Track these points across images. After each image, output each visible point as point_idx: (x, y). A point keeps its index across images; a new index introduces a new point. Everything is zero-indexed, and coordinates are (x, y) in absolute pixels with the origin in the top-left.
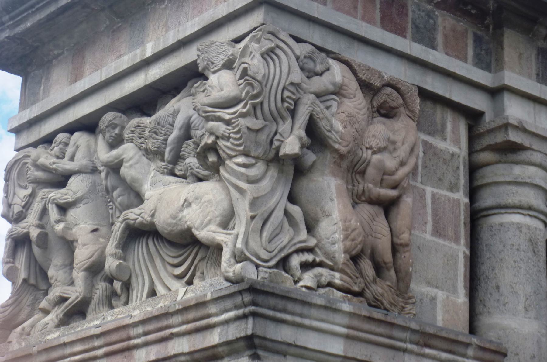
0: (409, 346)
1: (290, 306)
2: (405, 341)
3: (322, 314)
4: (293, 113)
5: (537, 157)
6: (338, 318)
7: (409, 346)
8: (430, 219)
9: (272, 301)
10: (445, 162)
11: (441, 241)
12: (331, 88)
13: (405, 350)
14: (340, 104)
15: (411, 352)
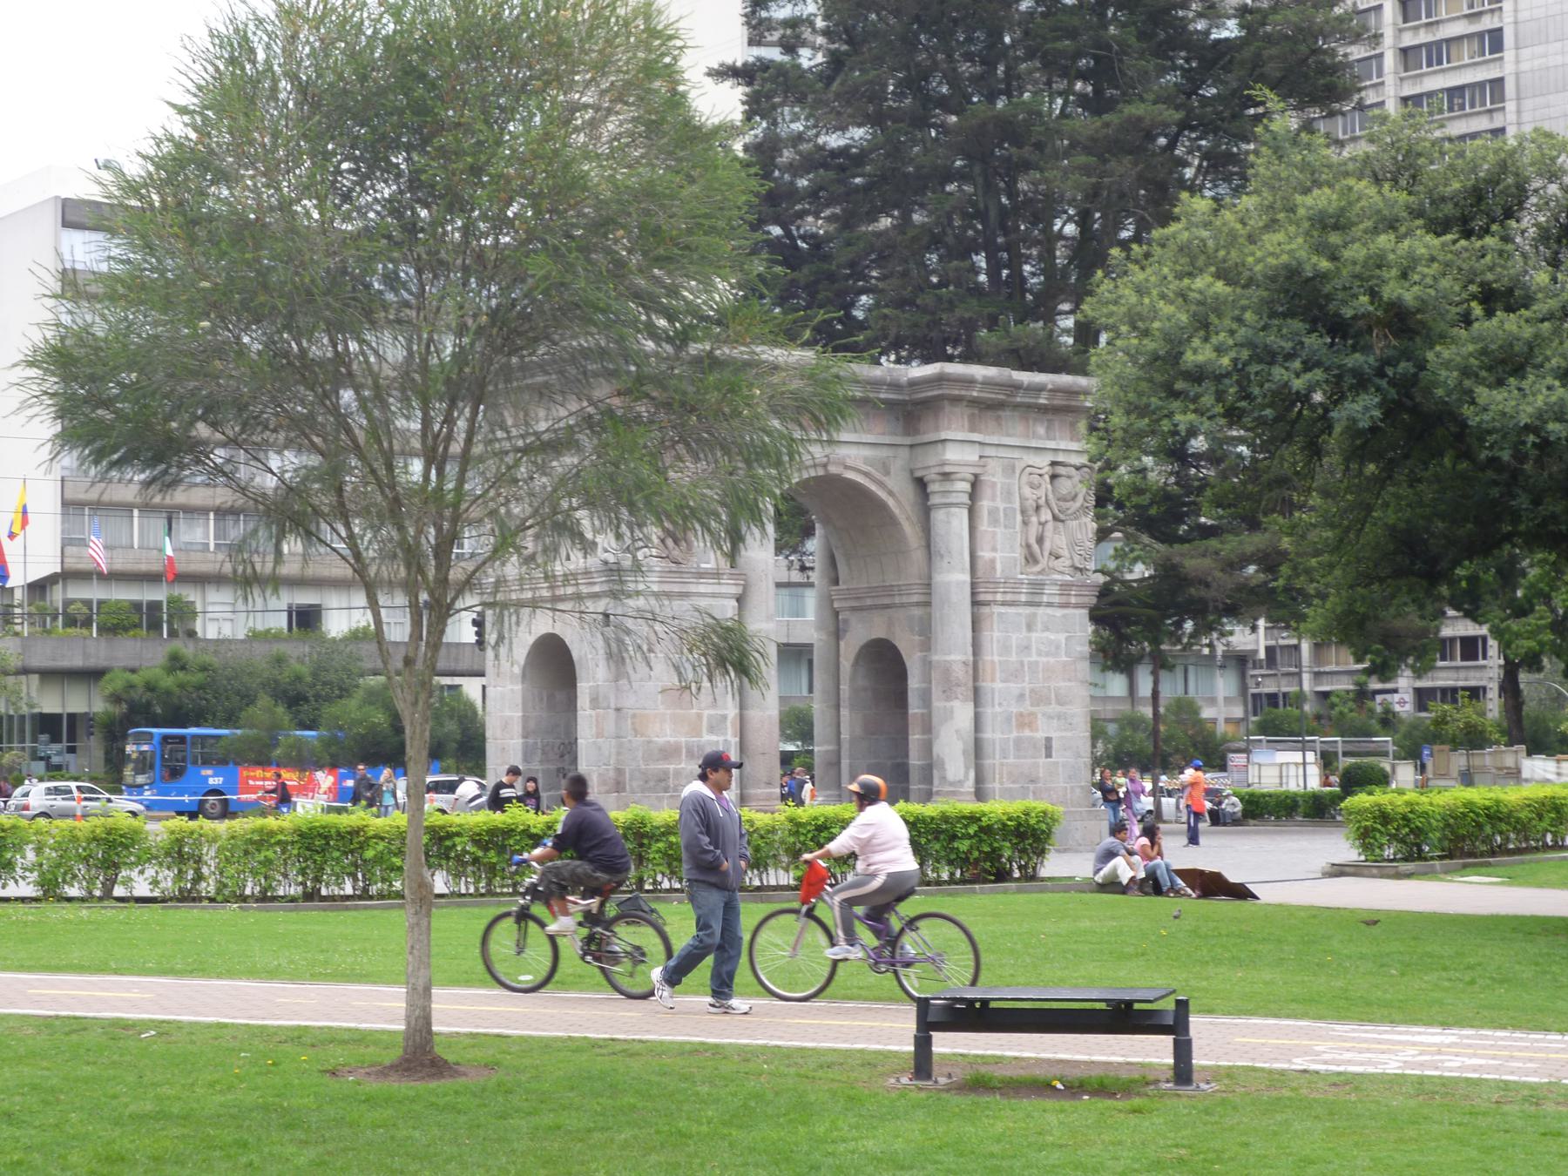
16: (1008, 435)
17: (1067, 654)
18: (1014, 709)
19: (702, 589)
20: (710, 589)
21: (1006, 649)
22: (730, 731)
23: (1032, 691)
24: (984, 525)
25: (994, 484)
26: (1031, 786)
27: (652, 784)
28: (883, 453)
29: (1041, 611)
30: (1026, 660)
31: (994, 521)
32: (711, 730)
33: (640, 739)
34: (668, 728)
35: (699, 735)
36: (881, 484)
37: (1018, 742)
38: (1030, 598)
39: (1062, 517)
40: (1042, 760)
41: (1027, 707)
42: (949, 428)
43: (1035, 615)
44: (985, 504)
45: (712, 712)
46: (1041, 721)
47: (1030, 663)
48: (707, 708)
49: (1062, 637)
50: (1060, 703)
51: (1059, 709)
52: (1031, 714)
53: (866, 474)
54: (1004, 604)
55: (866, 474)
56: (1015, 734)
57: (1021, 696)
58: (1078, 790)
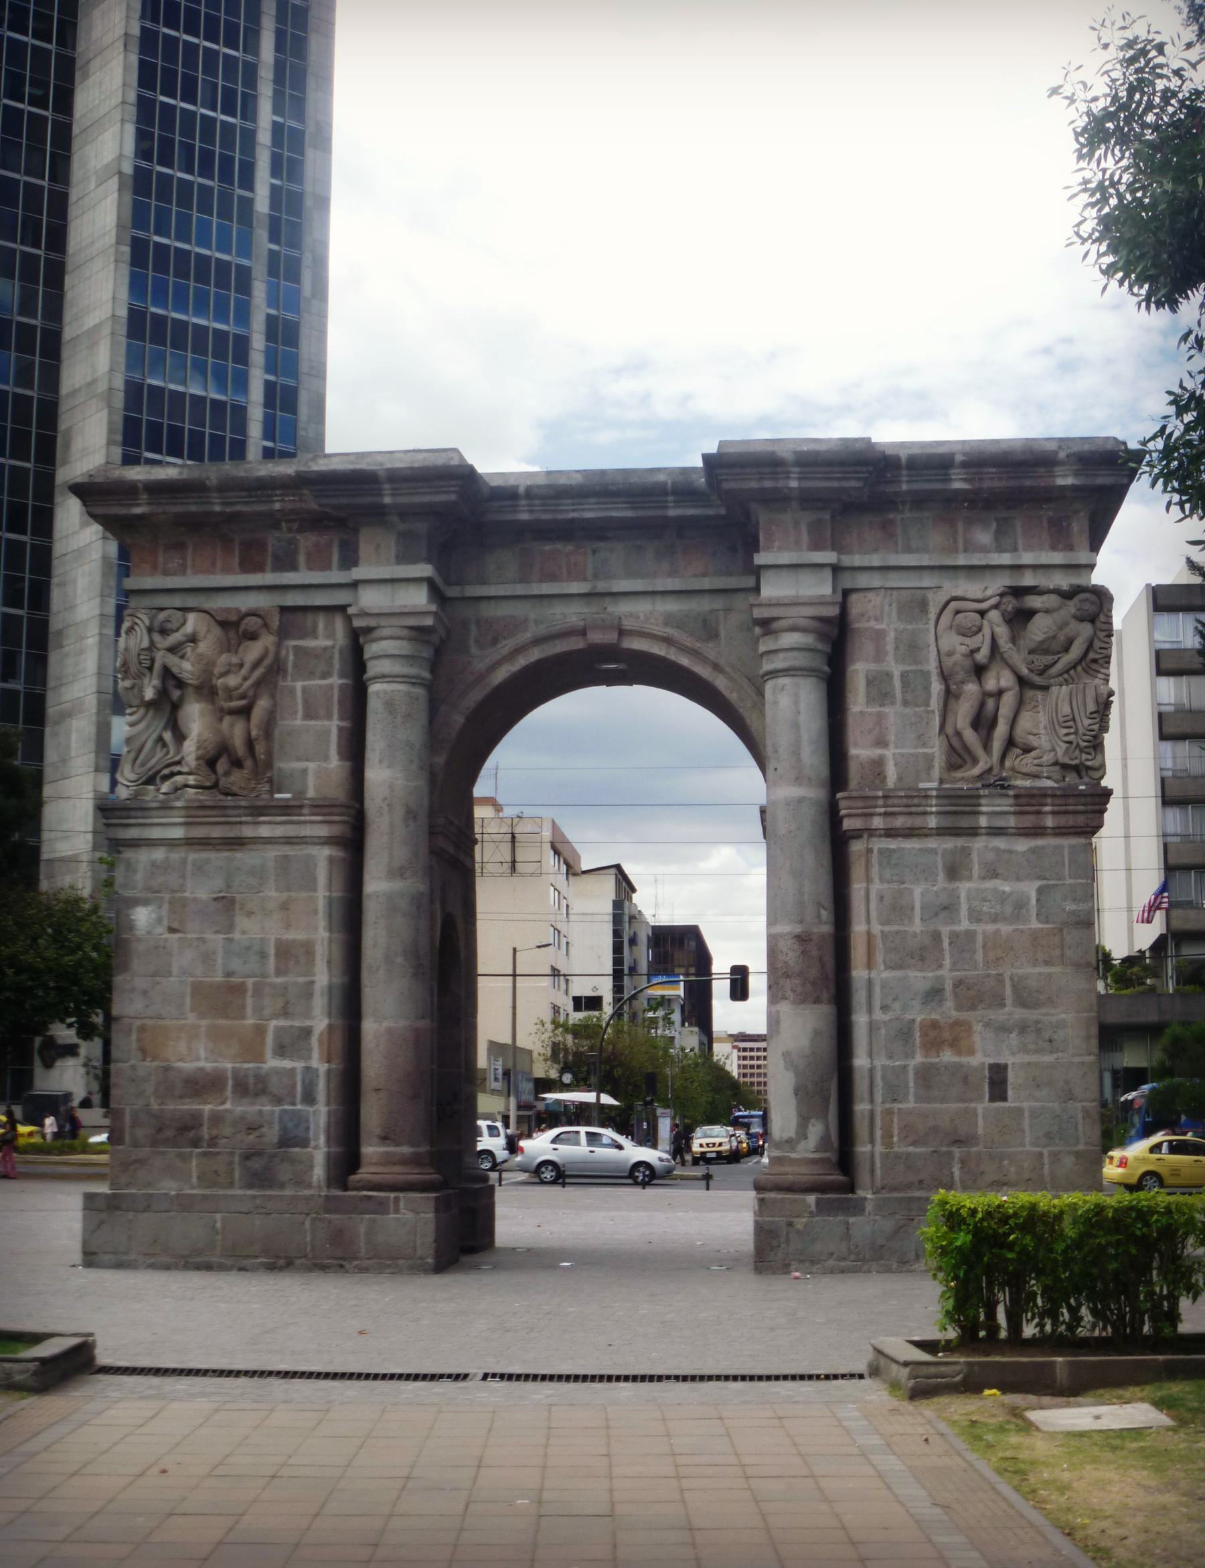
0: (244, 819)
1: (133, 813)
2: (239, 816)
3: (162, 813)
4: (150, 669)
5: (386, 632)
6: (175, 813)
7: (244, 819)
8: (300, 707)
9: (118, 813)
10: (317, 656)
11: (313, 723)
12: (184, 639)
13: (241, 823)
14: (194, 649)
15: (247, 823)
16: (908, 550)
17: (1042, 916)
18: (919, 1015)
19: (265, 831)
20: (279, 831)
21: (898, 909)
22: (316, 1054)
23: (958, 984)
24: (858, 703)
25: (880, 635)
26: (957, 1152)
27: (170, 1133)
28: (703, 605)
29: (979, 843)
30: (945, 931)
31: (879, 689)
32: (282, 1050)
33: (149, 1064)
34: (201, 1049)
35: (260, 1058)
36: (694, 653)
37: (926, 1076)
38: (947, 822)
39: (1038, 680)
40: (983, 1106)
41: (948, 1010)
42: (768, 548)
43: (966, 852)
44: (859, 671)
45: (282, 1023)
46: (980, 1037)
47: (954, 937)
48: (276, 1016)
49: (1030, 889)
50: (1023, 1001)
51: (1020, 1014)
52: (957, 1023)
53: (668, 641)
54: (890, 833)
55: (668, 641)
56: (919, 1059)
57: (934, 994)
58: (1069, 1161)
